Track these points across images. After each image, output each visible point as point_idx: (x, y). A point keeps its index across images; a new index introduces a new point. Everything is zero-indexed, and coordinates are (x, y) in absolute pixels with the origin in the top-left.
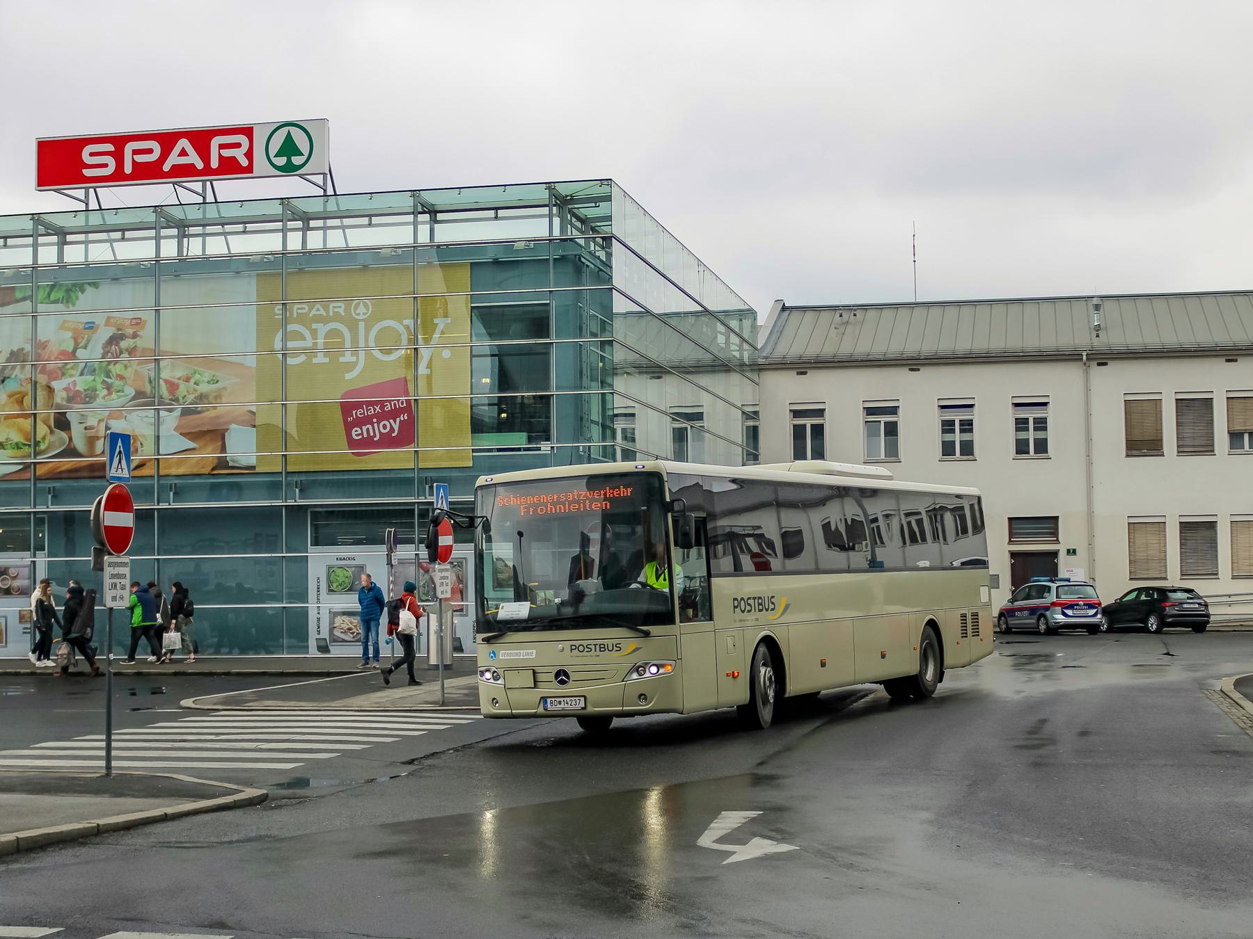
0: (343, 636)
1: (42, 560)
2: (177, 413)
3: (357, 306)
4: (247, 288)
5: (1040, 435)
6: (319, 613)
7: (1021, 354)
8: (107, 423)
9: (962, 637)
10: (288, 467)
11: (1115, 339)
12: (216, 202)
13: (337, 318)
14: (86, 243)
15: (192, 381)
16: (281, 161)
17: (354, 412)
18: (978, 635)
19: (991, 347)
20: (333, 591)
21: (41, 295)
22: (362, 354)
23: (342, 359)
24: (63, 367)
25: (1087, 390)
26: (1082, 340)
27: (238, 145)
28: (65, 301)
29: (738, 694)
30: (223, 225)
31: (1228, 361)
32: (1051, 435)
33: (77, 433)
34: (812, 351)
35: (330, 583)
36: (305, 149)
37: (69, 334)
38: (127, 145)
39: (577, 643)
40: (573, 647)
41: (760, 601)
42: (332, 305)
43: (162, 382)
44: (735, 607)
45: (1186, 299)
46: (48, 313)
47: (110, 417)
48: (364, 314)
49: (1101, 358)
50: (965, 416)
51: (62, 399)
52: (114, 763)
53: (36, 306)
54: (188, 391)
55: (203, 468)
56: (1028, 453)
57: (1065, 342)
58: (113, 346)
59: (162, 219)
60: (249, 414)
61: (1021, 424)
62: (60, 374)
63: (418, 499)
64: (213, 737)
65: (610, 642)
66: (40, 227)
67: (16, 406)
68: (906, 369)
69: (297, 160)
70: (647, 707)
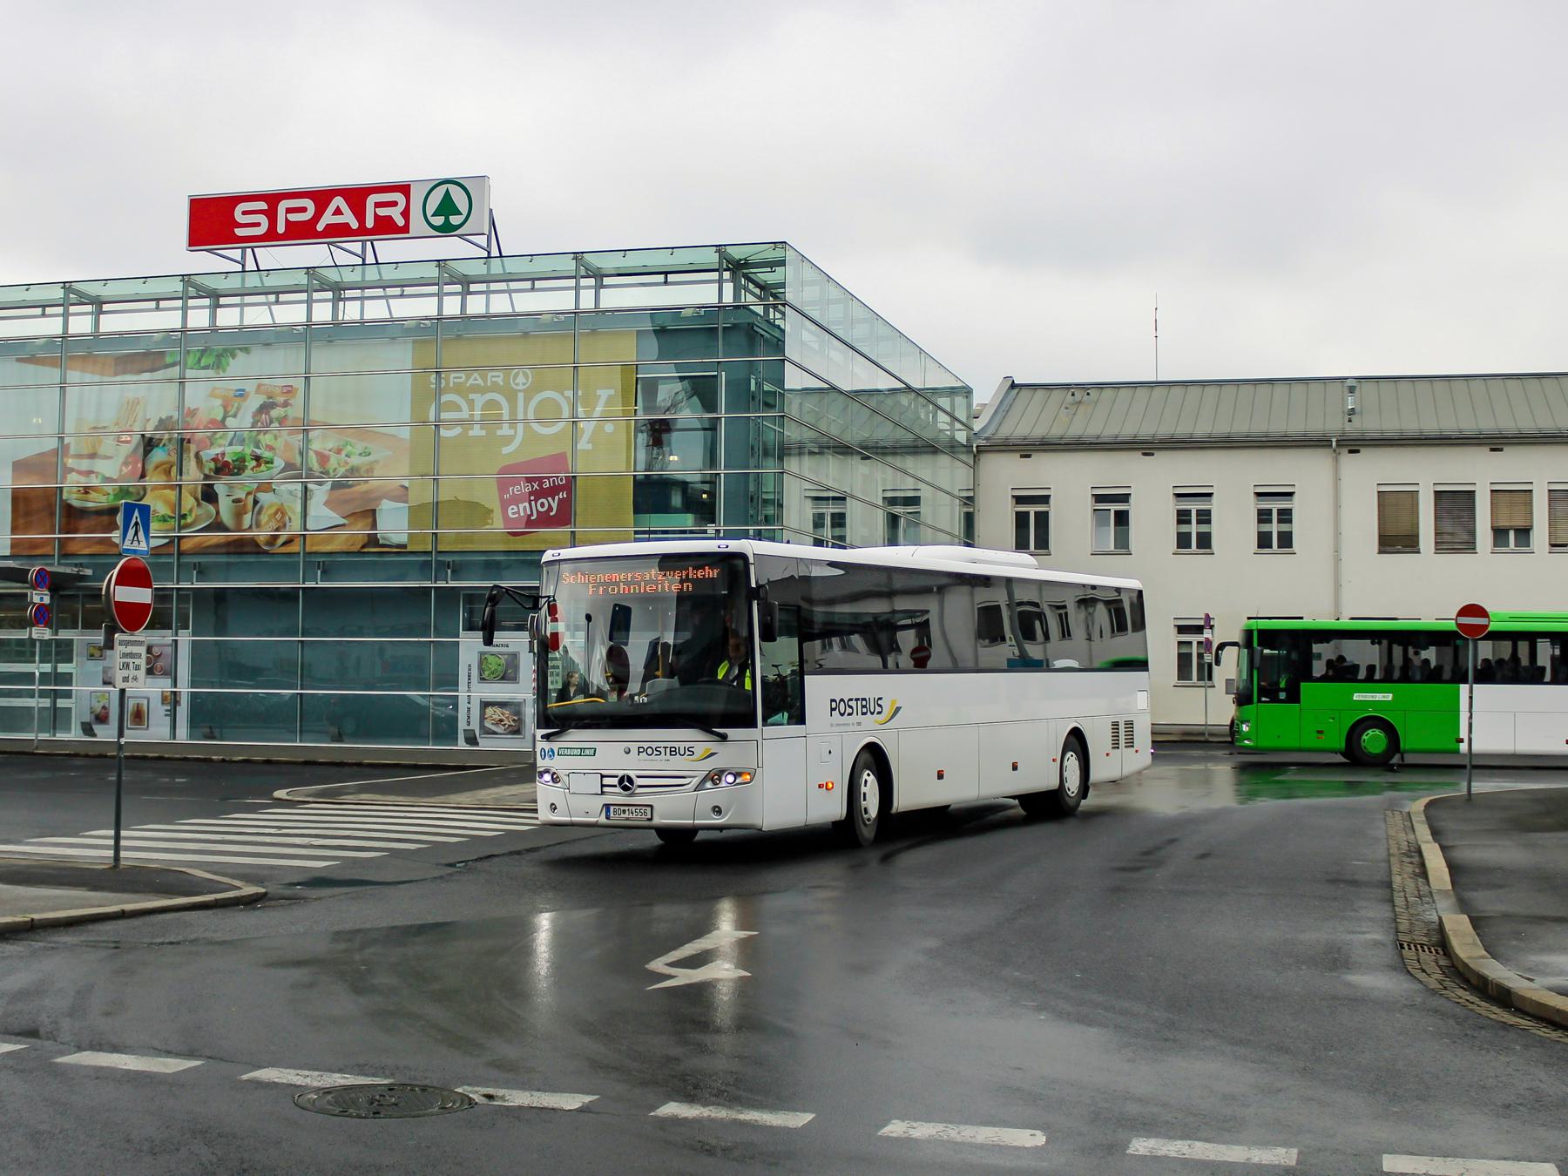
0: (494, 728)
1: (185, 638)
2: (328, 486)
3: (516, 375)
4: (401, 356)
5: (1204, 528)
6: (469, 703)
7: (1264, 439)
8: (255, 496)
9: (1113, 748)
10: (438, 546)
11: (1369, 424)
12: (377, 263)
13: (495, 388)
14: (362, 299)
15: (344, 453)
16: (439, 221)
17: (511, 489)
18: (1133, 746)
19: (1385, 427)
20: (484, 679)
21: (191, 360)
22: (520, 427)
23: (499, 433)
24: (212, 436)
25: (1337, 479)
26: (1334, 425)
27: (394, 204)
28: (215, 367)
29: (832, 808)
30: (384, 288)
31: (1492, 450)
32: (1297, 528)
33: (225, 504)
34: (1039, 432)
35: (481, 670)
36: (463, 208)
37: (219, 402)
38: (239, 205)
39: (646, 745)
40: (641, 750)
41: (864, 703)
42: (491, 374)
43: (311, 454)
44: (832, 709)
45: (1452, 383)
46: (196, 380)
47: (259, 490)
48: (524, 384)
49: (1354, 445)
50: (1283, 504)
51: (210, 469)
52: (123, 854)
53: (185, 371)
54: (339, 464)
55: (352, 545)
56: (1271, 547)
57: (1316, 425)
58: (264, 415)
59: (315, 282)
60: (401, 488)
61: (1264, 516)
62: (209, 444)
63: (436, 583)
64: (272, 831)
65: (682, 745)
66: (190, 289)
67: (165, 478)
68: (1139, 454)
69: (455, 220)
70: (723, 820)
